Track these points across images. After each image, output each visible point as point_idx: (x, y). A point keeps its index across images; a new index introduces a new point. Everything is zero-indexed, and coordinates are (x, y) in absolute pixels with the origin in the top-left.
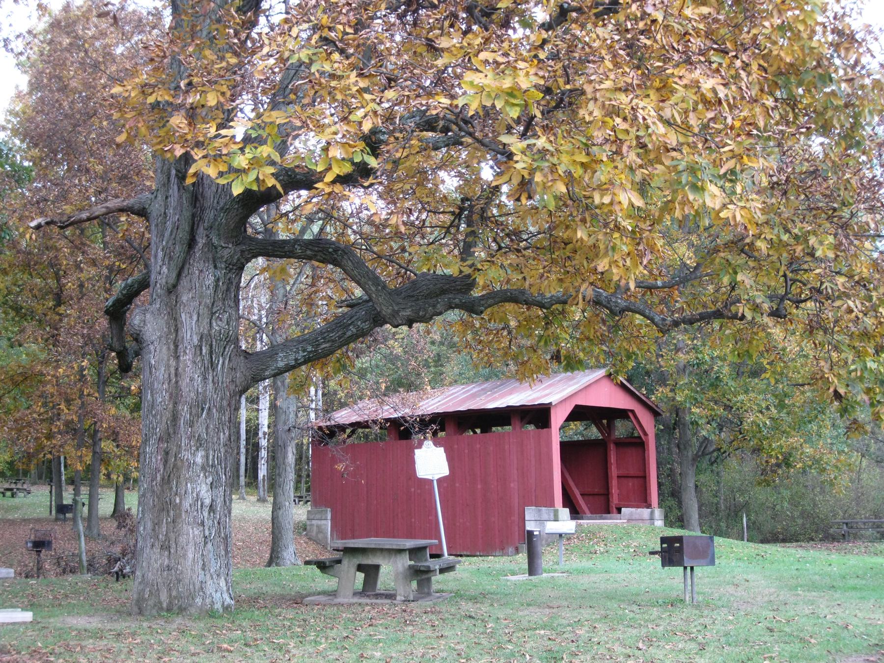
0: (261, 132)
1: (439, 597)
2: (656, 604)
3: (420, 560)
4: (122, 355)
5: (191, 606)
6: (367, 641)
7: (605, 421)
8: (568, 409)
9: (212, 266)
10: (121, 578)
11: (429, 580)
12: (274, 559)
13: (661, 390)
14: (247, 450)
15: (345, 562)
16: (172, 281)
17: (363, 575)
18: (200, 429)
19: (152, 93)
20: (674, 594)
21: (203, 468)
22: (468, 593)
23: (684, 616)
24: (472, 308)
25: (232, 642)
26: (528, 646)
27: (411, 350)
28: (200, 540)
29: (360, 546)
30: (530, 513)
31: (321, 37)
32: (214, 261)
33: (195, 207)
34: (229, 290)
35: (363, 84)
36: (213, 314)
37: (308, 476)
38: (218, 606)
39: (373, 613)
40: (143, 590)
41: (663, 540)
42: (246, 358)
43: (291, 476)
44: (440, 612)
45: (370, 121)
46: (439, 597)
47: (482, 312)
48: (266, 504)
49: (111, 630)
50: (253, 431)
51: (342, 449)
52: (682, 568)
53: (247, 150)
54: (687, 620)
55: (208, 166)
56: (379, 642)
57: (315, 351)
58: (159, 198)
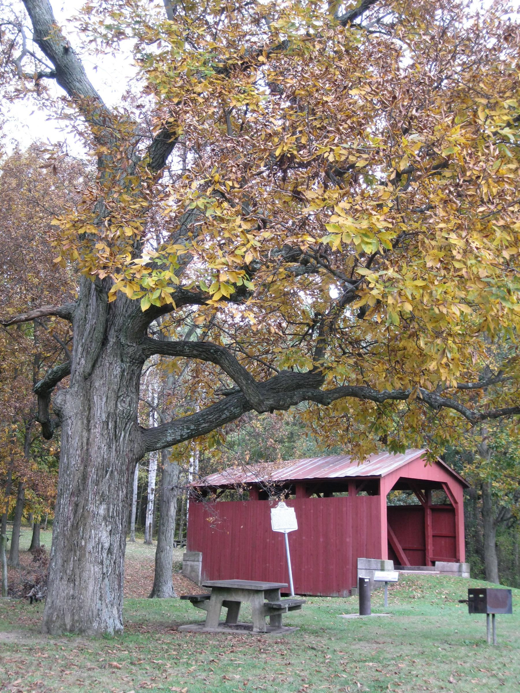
0: (165, 261)
1: (287, 630)
2: (463, 644)
3: (273, 599)
4: (45, 425)
5: (89, 628)
6: (229, 665)
7: (423, 491)
8: (394, 481)
9: (119, 360)
10: (34, 601)
11: (279, 616)
12: (156, 592)
13: (468, 466)
14: (138, 503)
15: (213, 598)
16: (88, 370)
17: (227, 609)
18: (104, 487)
19: (81, 227)
20: (478, 636)
21: (105, 518)
22: (310, 628)
23: (486, 655)
24: (321, 399)
25: (121, 660)
26: (359, 675)
27: (270, 429)
28: (99, 576)
29: (226, 586)
30: (362, 563)
31: (214, 190)
32: (121, 356)
33: (109, 314)
34: (132, 379)
35: (246, 226)
36: (118, 397)
37: (185, 525)
38: (111, 630)
39: (234, 641)
40: (52, 614)
41: (471, 591)
42: (142, 433)
43: (172, 525)
44: (288, 643)
45: (251, 255)
46: (287, 630)
47: (329, 404)
48: (151, 546)
49: (25, 645)
50: (143, 487)
51: (213, 506)
52: (484, 615)
53: (154, 274)
54: (489, 659)
55: (125, 286)
56: (239, 667)
57: (197, 429)
58: (82, 306)
